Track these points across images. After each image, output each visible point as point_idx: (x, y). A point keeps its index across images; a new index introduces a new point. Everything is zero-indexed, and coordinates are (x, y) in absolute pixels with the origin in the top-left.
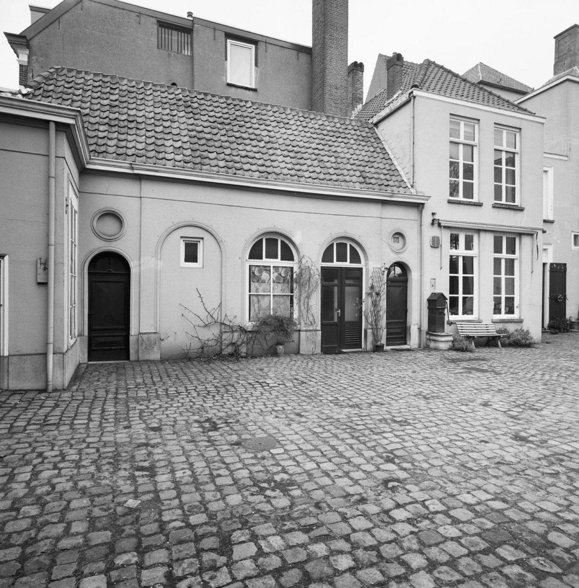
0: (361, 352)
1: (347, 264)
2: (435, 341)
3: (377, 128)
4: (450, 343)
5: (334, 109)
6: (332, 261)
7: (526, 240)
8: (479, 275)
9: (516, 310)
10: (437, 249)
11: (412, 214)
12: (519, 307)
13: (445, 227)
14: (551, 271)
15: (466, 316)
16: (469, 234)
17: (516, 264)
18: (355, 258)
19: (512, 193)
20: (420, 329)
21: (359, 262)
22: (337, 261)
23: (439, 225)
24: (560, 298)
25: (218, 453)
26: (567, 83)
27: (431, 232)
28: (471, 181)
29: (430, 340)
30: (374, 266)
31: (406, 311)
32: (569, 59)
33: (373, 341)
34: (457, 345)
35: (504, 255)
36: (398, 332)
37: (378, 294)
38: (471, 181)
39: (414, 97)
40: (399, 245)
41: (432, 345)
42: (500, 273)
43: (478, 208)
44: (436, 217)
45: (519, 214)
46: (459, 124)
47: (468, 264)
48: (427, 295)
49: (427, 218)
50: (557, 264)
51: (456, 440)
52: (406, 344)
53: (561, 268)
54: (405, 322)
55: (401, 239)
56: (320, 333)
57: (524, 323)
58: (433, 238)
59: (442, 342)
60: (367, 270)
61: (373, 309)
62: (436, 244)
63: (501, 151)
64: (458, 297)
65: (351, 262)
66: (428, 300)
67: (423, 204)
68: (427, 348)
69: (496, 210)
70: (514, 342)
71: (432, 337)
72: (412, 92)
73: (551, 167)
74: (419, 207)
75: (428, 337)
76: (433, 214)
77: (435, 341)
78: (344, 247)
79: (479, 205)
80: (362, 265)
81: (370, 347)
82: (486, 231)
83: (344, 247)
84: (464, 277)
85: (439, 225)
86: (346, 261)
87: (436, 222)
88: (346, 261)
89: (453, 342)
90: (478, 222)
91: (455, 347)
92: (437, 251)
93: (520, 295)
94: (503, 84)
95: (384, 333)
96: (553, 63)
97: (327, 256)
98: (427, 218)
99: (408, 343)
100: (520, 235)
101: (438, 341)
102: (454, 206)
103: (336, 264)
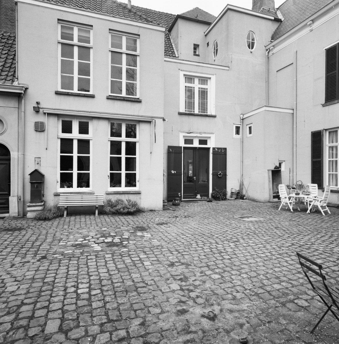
5: (9, 26)
10: (42, 133)
14: (213, 154)
15: (79, 188)
19: (131, 89)
24: (220, 174)
25: (97, 267)
28: (121, 80)
32: (259, 3)
38: (121, 80)
45: (137, 105)
46: (72, 29)
47: (84, 145)
48: (30, 169)
50: (218, 149)
51: (279, 258)
53: (221, 151)
57: (142, 196)
63: (121, 53)
64: (121, 174)
69: (110, 102)
73: (213, 75)
74: (18, 97)
76: (38, 103)
79: (92, 97)
84: (126, 158)
94: (199, 18)
98: (29, 105)
100: (140, 122)
102: (62, 98)
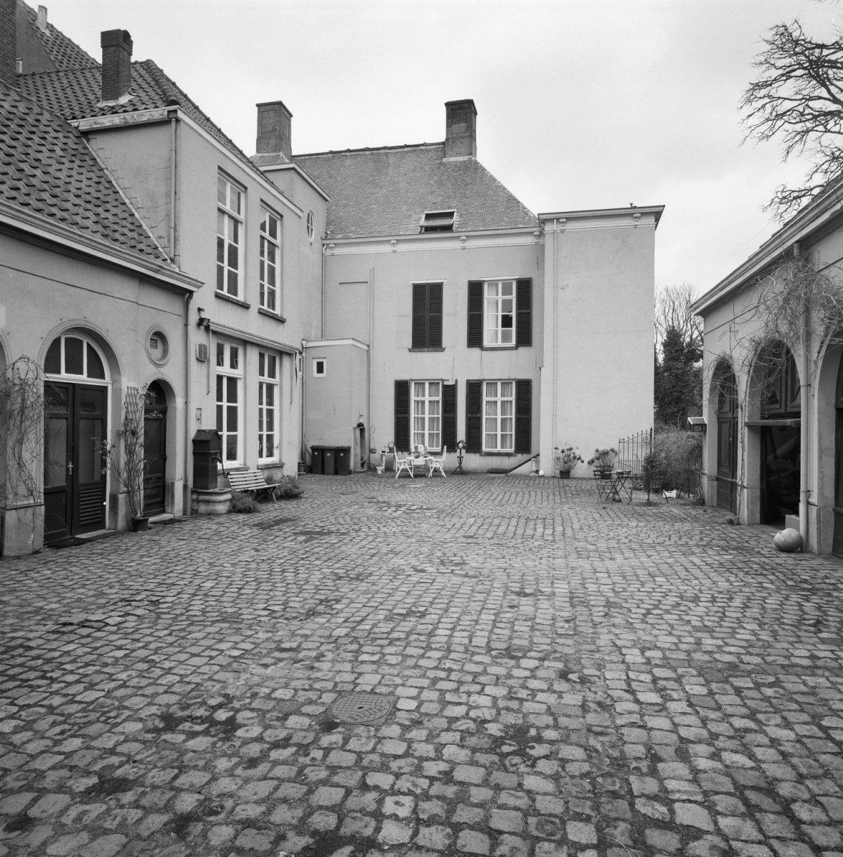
0: (105, 536)
1: (83, 378)
2: (208, 502)
3: (88, 140)
4: (228, 504)
6: (59, 372)
7: (286, 360)
8: (245, 403)
9: (276, 452)
11: (174, 305)
12: (280, 447)
13: (215, 333)
16: (235, 346)
17: (276, 391)
18: (96, 371)
20: (185, 487)
21: (102, 376)
22: (67, 371)
23: (207, 329)
26: (293, 172)
27: (198, 338)
29: (198, 501)
30: (127, 383)
31: (165, 459)
33: (126, 514)
34: (240, 505)
35: (266, 379)
36: (159, 494)
37: (134, 433)
39: (178, 121)
40: (157, 353)
41: (203, 508)
42: (221, 401)
43: (240, 310)
44: (204, 315)
45: (281, 327)
48: (192, 434)
49: (194, 318)
52: (164, 512)
54: (163, 478)
55: (160, 345)
56: (43, 508)
58: (200, 345)
59: (220, 502)
60: (117, 392)
61: (120, 456)
62: (203, 358)
65: (89, 376)
66: (194, 441)
67: (191, 292)
68: (195, 513)
70: (285, 492)
71: (202, 497)
72: (175, 111)
75: (195, 496)
77: (208, 502)
78: (82, 346)
80: (107, 381)
81: (121, 523)
82: (252, 344)
83: (82, 346)
85: (207, 329)
86: (81, 373)
87: (205, 323)
88: (81, 373)
89: (231, 500)
90: (246, 331)
91: (235, 509)
92: (204, 366)
93: (281, 432)
95: (140, 495)
96: (255, 137)
97: (51, 364)
99: (168, 509)
101: (214, 502)
103: (64, 376)
